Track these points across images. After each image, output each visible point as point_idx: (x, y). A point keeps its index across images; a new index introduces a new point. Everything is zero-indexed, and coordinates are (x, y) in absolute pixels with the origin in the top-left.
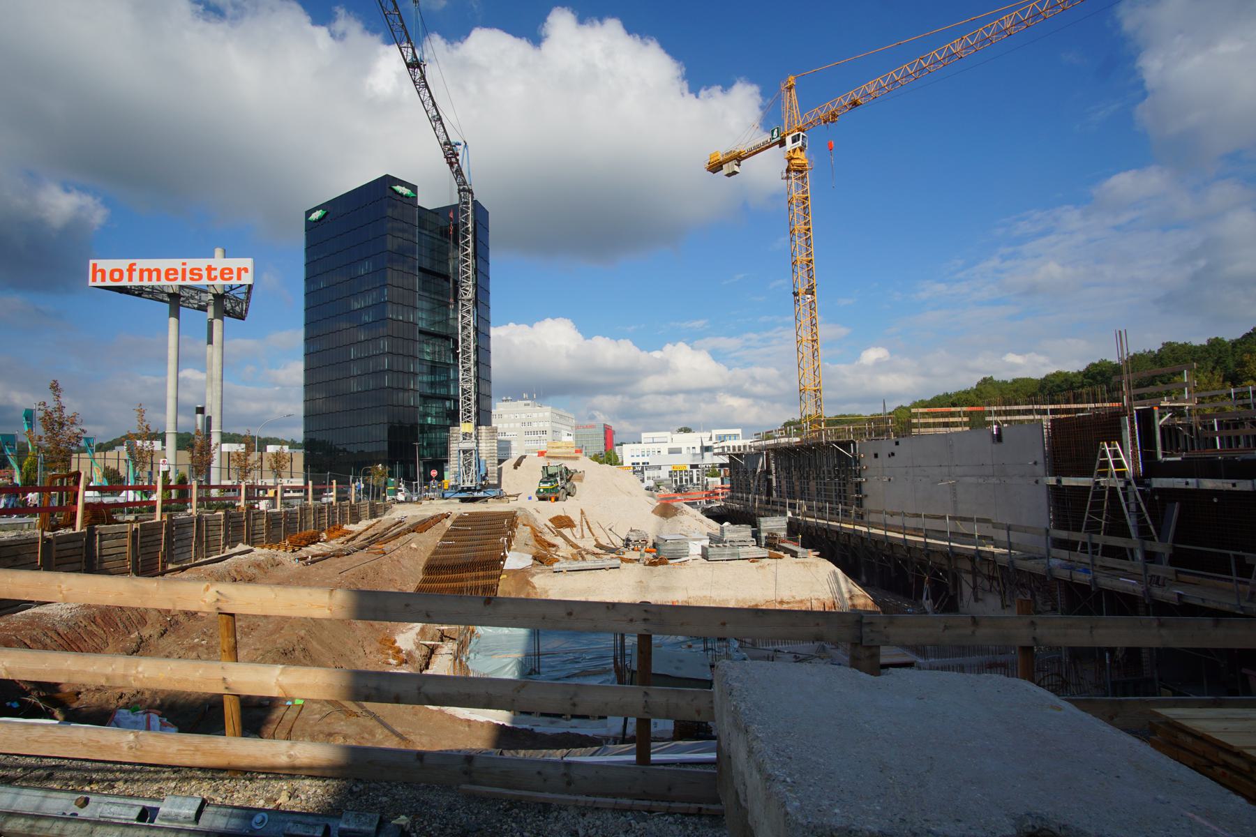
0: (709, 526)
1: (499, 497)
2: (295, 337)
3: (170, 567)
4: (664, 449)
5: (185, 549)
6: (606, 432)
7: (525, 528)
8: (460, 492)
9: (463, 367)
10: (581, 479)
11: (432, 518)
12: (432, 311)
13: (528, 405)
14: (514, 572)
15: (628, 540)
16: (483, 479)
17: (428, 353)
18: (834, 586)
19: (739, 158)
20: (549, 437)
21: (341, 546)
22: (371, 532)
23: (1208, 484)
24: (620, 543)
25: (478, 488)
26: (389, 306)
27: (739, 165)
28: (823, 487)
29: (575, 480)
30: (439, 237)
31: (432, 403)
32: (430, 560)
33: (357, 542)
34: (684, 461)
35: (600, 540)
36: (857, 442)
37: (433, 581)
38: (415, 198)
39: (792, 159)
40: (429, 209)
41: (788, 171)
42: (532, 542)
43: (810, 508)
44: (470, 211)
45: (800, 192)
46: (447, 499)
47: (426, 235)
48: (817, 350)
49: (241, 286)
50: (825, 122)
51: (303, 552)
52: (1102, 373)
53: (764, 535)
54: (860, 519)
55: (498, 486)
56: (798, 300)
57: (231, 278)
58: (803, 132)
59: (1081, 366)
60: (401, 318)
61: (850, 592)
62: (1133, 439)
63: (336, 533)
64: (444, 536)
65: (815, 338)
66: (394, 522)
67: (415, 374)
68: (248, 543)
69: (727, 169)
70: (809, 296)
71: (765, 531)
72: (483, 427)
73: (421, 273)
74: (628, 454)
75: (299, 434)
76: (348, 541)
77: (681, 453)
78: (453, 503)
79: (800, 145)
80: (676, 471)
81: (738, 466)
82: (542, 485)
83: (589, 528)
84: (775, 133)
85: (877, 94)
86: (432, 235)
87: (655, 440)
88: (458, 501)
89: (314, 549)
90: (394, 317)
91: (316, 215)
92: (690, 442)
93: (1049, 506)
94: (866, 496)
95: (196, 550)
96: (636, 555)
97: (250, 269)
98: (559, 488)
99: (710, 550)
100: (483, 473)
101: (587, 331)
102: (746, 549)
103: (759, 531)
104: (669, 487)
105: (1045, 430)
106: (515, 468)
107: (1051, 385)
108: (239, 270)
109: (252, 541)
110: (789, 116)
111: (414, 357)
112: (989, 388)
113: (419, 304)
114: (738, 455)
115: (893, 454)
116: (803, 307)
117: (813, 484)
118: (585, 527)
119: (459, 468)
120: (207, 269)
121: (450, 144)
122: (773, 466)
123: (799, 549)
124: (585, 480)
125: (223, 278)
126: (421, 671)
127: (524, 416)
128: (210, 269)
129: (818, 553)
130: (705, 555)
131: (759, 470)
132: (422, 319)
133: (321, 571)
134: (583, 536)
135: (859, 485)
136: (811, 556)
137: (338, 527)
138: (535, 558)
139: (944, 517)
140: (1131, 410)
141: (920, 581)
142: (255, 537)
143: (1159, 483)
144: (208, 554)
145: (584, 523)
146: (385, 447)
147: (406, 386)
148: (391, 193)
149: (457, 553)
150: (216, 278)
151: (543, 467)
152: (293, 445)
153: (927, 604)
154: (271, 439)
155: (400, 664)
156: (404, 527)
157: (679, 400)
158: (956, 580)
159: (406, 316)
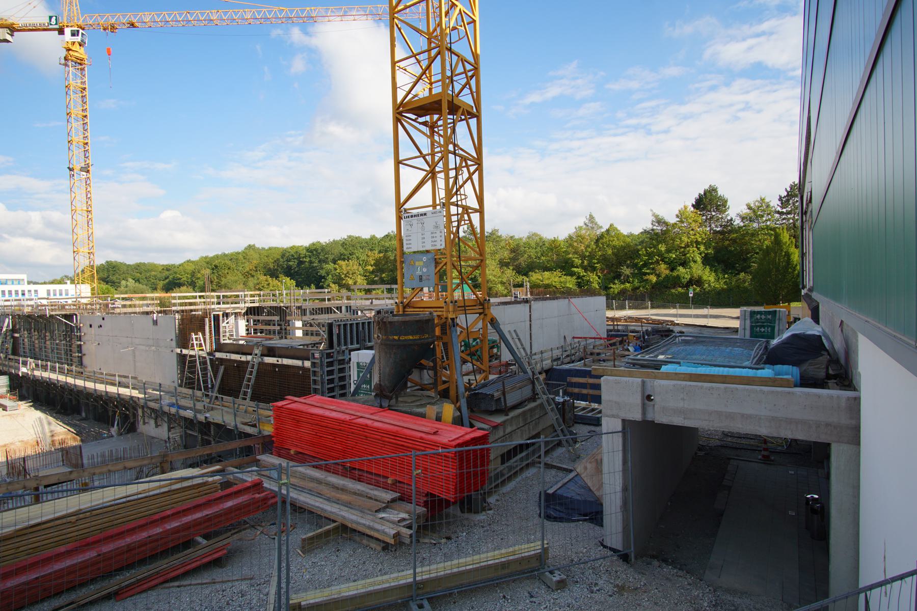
18: (39, 429)
27: (12, 35)
28: (55, 346)
36: (78, 315)
43: (37, 365)
52: (316, 250)
54: (80, 375)
56: (73, 175)
58: (83, 29)
62: (210, 331)
65: (90, 209)
70: (85, 173)
79: (79, 40)
84: (54, 19)
93: (178, 365)
94: (84, 355)
105: (177, 321)
107: (288, 254)
112: (252, 252)
115: (101, 326)
131: (4, 329)
135: (80, 346)
136: (24, 406)
139: (115, 375)
140: (210, 315)
143: (218, 355)
153: (114, 430)
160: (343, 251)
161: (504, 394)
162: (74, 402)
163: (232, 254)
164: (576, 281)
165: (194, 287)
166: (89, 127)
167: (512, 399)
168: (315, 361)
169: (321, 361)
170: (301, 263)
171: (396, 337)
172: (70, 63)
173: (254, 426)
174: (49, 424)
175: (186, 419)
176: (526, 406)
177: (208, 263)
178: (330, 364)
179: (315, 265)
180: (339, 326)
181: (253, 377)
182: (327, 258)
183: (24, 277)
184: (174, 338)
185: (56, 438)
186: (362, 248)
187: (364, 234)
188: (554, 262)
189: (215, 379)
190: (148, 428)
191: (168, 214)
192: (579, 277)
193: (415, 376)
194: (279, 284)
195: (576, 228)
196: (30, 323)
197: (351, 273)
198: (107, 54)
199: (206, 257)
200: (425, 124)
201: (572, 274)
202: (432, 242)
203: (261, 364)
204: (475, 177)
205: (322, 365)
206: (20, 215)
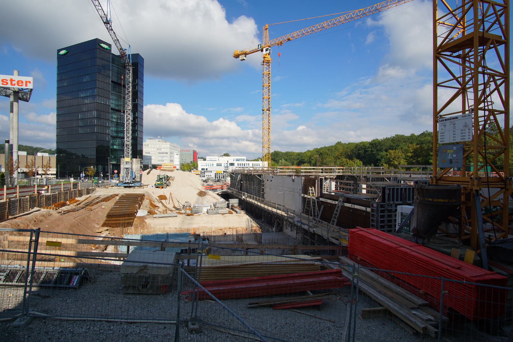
1: (141, 186)
2: (53, 103)
3: (10, 217)
4: (215, 163)
5: (15, 210)
6: (194, 153)
7: (147, 200)
8: (124, 184)
9: (126, 136)
10: (173, 180)
11: (111, 196)
12: (117, 100)
13: (160, 141)
14: (140, 217)
15: (184, 206)
17: (115, 118)
18: (247, 223)
19: (246, 54)
21: (74, 207)
22: (87, 201)
25: (132, 182)
27: (246, 57)
29: (171, 180)
32: (109, 213)
33: (81, 205)
34: (221, 169)
35: (175, 205)
37: (109, 221)
38: (110, 50)
40: (117, 55)
41: (263, 62)
42: (149, 206)
44: (131, 74)
45: (268, 71)
46: (119, 186)
49: (27, 89)
50: (278, 45)
51: (61, 210)
52: (375, 144)
53: (230, 205)
55: (140, 181)
57: (22, 85)
58: (270, 47)
60: (103, 103)
61: (251, 225)
62: (318, 186)
63: (73, 201)
64: (115, 204)
66: (96, 197)
67: (109, 127)
68: (38, 207)
69: (241, 57)
70: (268, 112)
71: (231, 204)
72: (134, 159)
73: (113, 83)
74: (201, 164)
75: (54, 146)
76: (78, 205)
77: (221, 166)
78: (121, 188)
80: (218, 173)
82: (157, 182)
83: (172, 200)
84: (260, 46)
86: (118, 67)
87: (212, 160)
88: (123, 187)
89: (64, 208)
90: (100, 102)
91: (63, 52)
92: (224, 160)
95: (19, 210)
97: (32, 82)
98: (164, 184)
100: (134, 177)
101: (187, 109)
102: (222, 210)
106: (148, 174)
107: (359, 147)
108: (26, 82)
109: (39, 206)
110: (265, 40)
111: (109, 120)
112: (339, 146)
113: (111, 97)
114: (233, 173)
116: (266, 116)
118: (171, 200)
119: (124, 174)
120: (10, 80)
121: (122, 49)
124: (174, 181)
125: (18, 85)
126: (103, 251)
127: (158, 146)
128: (12, 80)
129: (245, 212)
131: (238, 180)
132: (113, 103)
133: (67, 218)
135: (263, 189)
137: (73, 199)
138: (148, 212)
140: (318, 178)
142: (41, 204)
143: (321, 199)
144: (23, 212)
146: (95, 157)
148: (98, 46)
150: (15, 85)
151: (158, 175)
152: (50, 152)
154: (39, 148)
155: (95, 249)
156: (100, 199)
157: (225, 142)
163: (329, 147)
169: (377, 209)
170: (366, 151)
171: (430, 200)
173: (337, 239)
174: (251, 222)
175: (304, 230)
177: (317, 152)
179: (374, 152)
181: (338, 213)
182: (382, 149)
183: (245, 158)
184: (301, 189)
189: (319, 211)
190: (288, 231)
191: (301, 128)
194: (353, 163)
196: (246, 177)
197: (397, 157)
199: (317, 149)
200: (458, 57)
202: (462, 136)
203: (343, 207)
204: (502, 88)
205: (377, 211)
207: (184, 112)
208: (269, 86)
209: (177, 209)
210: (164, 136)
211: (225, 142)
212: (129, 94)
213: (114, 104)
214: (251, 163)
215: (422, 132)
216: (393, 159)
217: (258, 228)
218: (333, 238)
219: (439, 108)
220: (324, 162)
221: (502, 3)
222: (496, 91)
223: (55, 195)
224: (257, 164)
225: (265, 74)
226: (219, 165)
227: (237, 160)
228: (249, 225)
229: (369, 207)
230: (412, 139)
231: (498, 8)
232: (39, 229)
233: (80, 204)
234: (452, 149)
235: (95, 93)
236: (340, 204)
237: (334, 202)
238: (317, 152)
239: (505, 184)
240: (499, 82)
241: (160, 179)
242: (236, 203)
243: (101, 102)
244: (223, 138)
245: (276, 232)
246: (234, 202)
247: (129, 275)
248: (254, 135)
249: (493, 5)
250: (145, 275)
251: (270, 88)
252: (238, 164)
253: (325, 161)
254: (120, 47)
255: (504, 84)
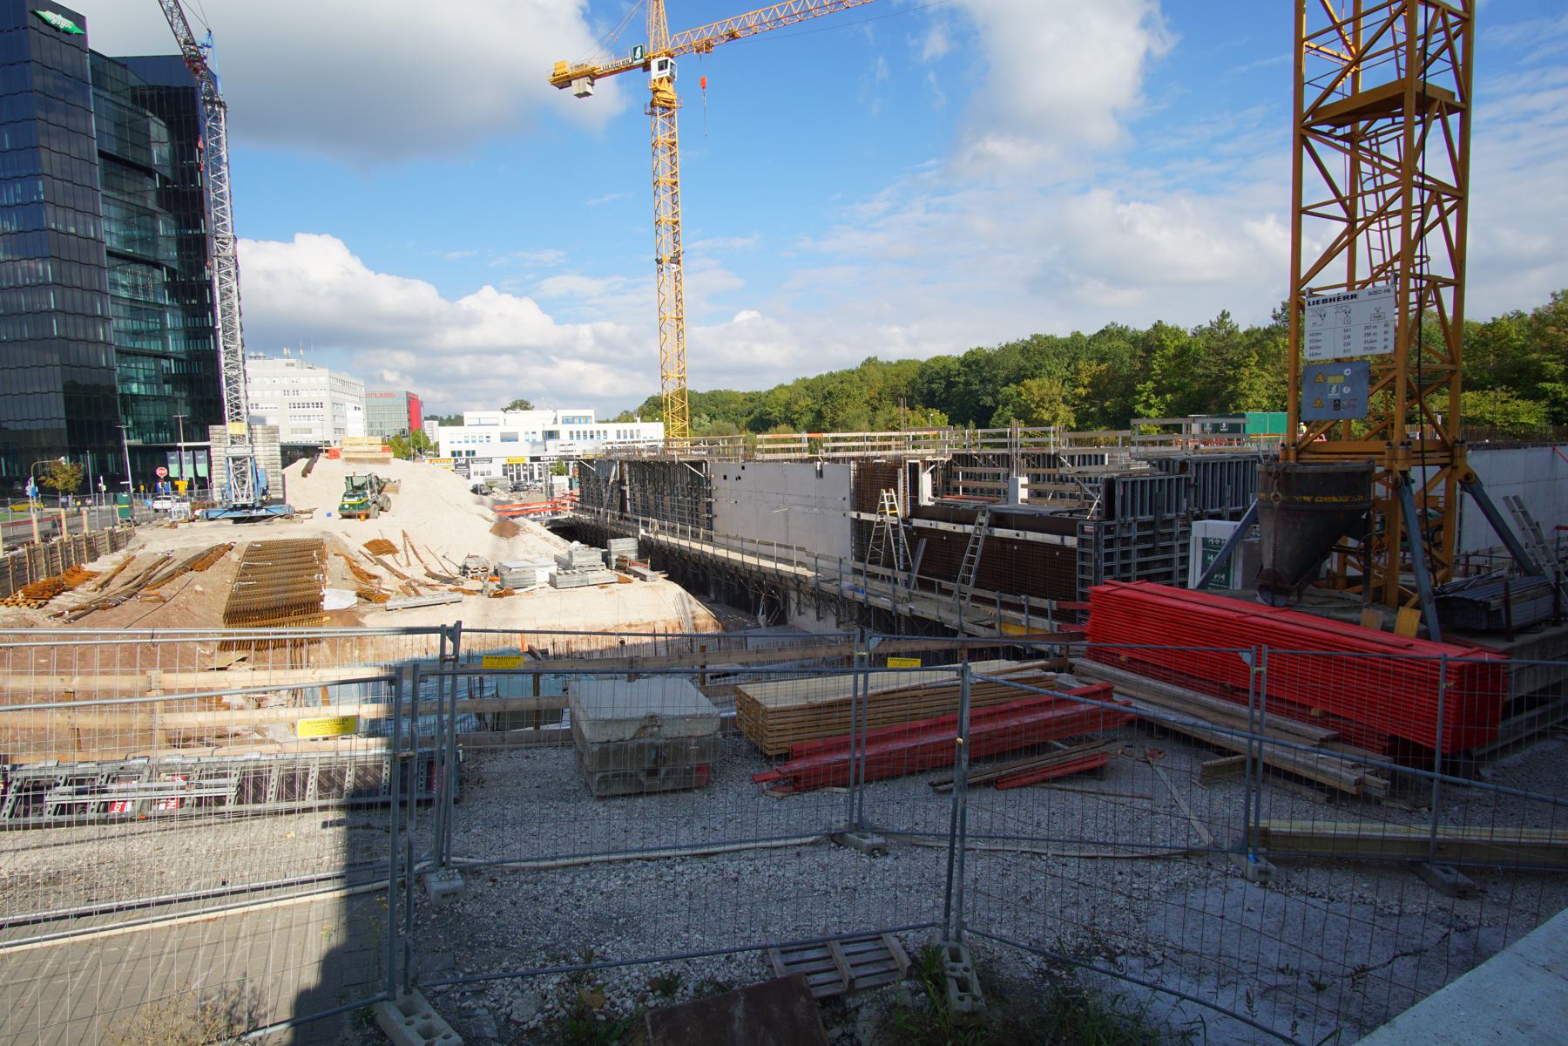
0: (556, 544)
4: (495, 433)
6: (409, 403)
8: (231, 510)
10: (396, 491)
11: (211, 550)
12: (126, 223)
13: (293, 365)
15: (465, 567)
16: (264, 493)
17: (124, 286)
18: (680, 607)
19: (593, 76)
20: (327, 410)
21: (95, 595)
23: (943, 526)
24: (455, 571)
25: (258, 505)
26: (50, 210)
27: (592, 85)
29: (389, 491)
30: (130, 105)
31: (136, 362)
34: (520, 452)
38: (82, 38)
39: (658, 91)
40: (109, 55)
41: (653, 105)
42: (351, 576)
43: (662, 527)
46: (212, 519)
47: (107, 99)
48: (682, 330)
52: (977, 363)
53: (614, 557)
54: (709, 540)
55: (282, 501)
59: (960, 353)
60: (72, 230)
63: (77, 577)
67: (105, 319)
69: (578, 86)
81: (588, 472)
82: (346, 500)
83: (415, 553)
84: (638, 52)
85: (757, 29)
90: (60, 227)
92: (520, 422)
96: (477, 585)
99: (558, 577)
102: (595, 574)
103: (609, 553)
104: (503, 488)
106: (304, 475)
114: (588, 461)
116: (669, 283)
117: (667, 499)
118: (411, 553)
121: (194, 44)
122: (627, 477)
123: (647, 572)
127: (286, 381)
130: (553, 582)
131: (612, 480)
134: (409, 564)
135: (709, 504)
136: (659, 579)
138: (359, 595)
141: (758, 597)
143: (917, 522)
145: (409, 547)
146: (63, 424)
147: (91, 337)
148: (33, 21)
149: (267, 594)
153: (761, 618)
157: (506, 364)
158: (786, 598)
159: (81, 227)
160: (1023, 362)
161: (1507, 603)
162: (701, 579)
163: (842, 374)
164: (1547, 409)
165: (794, 426)
166: (679, 198)
167: (1519, 615)
168: (1086, 537)
169: (1097, 538)
170: (951, 385)
171: (1308, 499)
172: (658, 110)
173: (991, 627)
174: (690, 602)
175: (878, 610)
176: (1543, 630)
177: (807, 388)
178: (1109, 543)
179: (974, 387)
180: (1125, 483)
181: (977, 558)
182: (995, 376)
183: (590, 413)
184: (848, 497)
185: (698, 621)
186: (1056, 355)
187: (1061, 329)
188: (1490, 371)
189: (913, 558)
190: (806, 620)
191: (744, 316)
192: (1555, 402)
193: (1332, 563)
194: (923, 420)
195: (1553, 295)
196: (644, 472)
197: (1047, 400)
198: (700, 87)
199: (804, 380)
200: (1344, 138)
201: (1537, 396)
202: (1366, 342)
203: (990, 539)
204: (1452, 219)
205: (1097, 545)
206: (567, 330)
207: (355, 264)
208: (675, 184)
209: (448, 581)
210: (306, 347)
211: (506, 364)
212: (222, 204)
213: (117, 235)
214: (612, 428)
215: (1102, 327)
216: (1037, 406)
217: (711, 621)
218: (975, 623)
219: (1306, 267)
220: (839, 419)
221: (1458, 7)
222: (1439, 227)
223: (19, 557)
224: (632, 431)
225: (660, 146)
226: (508, 438)
227: (567, 421)
228: (686, 614)
229: (1073, 535)
230: (1073, 348)
231: (1451, 19)
232: (459, 623)
233: (107, 583)
234: (1341, 374)
235: (39, 196)
236: (985, 531)
237: (959, 529)
238: (807, 388)
239: (1452, 457)
240: (1447, 206)
241: (356, 490)
242: (629, 551)
243: (66, 226)
244: (497, 351)
245: (768, 626)
246: (624, 547)
247: (612, 745)
248: (600, 340)
249: (1443, 11)
250: (653, 740)
251: (678, 189)
252: (571, 433)
253: (841, 416)
254: (185, 34)
255: (1455, 212)
